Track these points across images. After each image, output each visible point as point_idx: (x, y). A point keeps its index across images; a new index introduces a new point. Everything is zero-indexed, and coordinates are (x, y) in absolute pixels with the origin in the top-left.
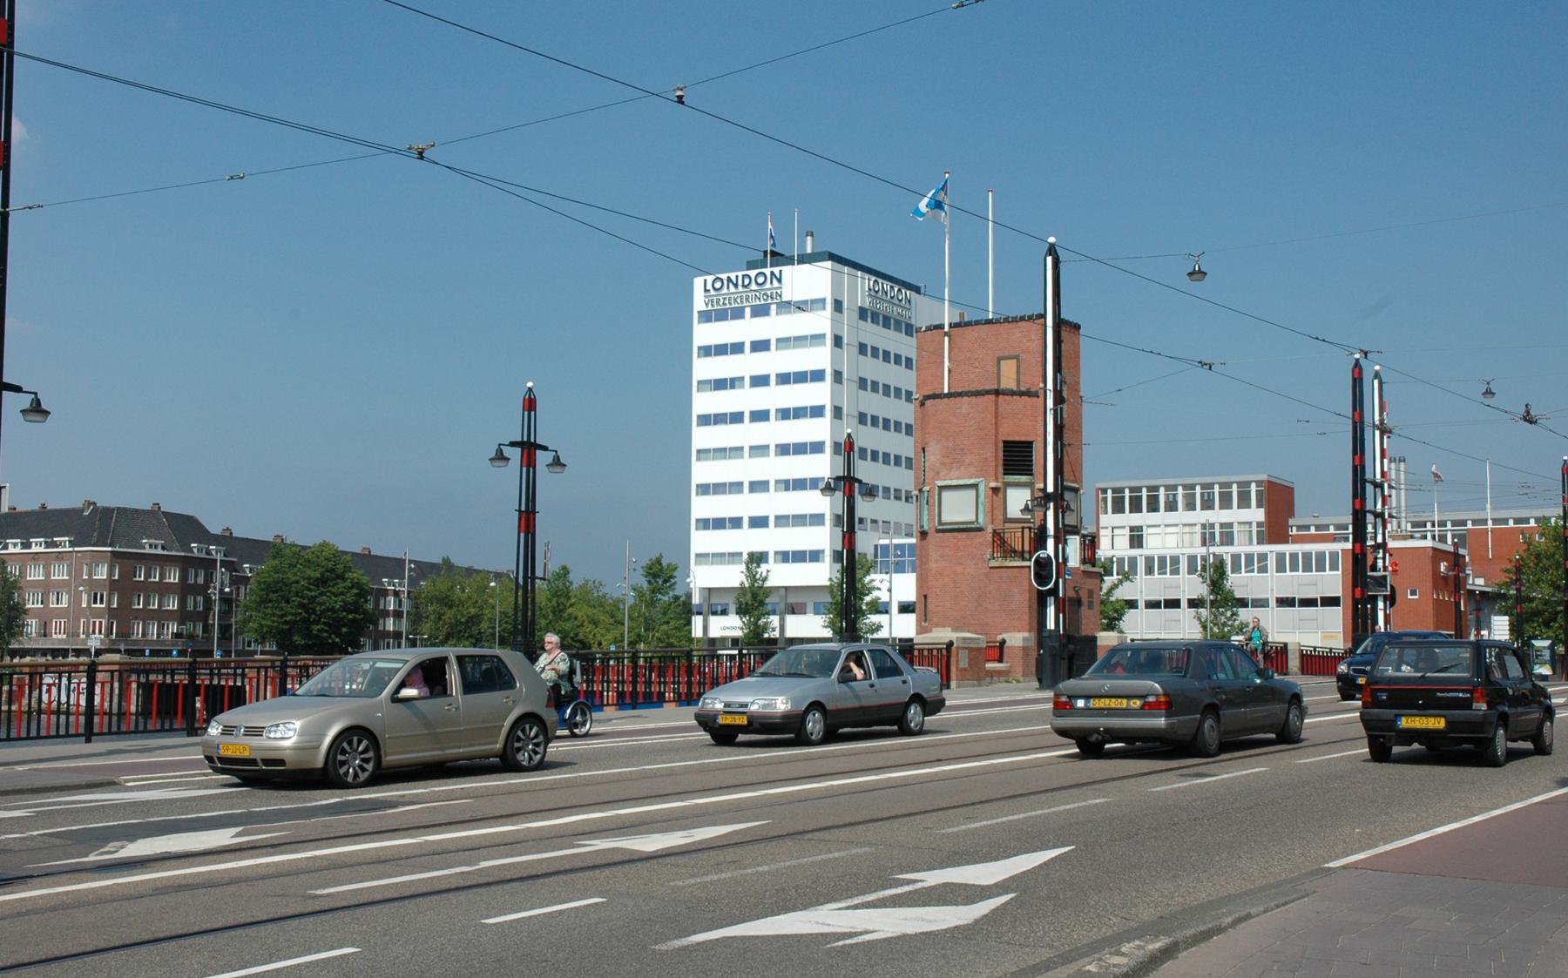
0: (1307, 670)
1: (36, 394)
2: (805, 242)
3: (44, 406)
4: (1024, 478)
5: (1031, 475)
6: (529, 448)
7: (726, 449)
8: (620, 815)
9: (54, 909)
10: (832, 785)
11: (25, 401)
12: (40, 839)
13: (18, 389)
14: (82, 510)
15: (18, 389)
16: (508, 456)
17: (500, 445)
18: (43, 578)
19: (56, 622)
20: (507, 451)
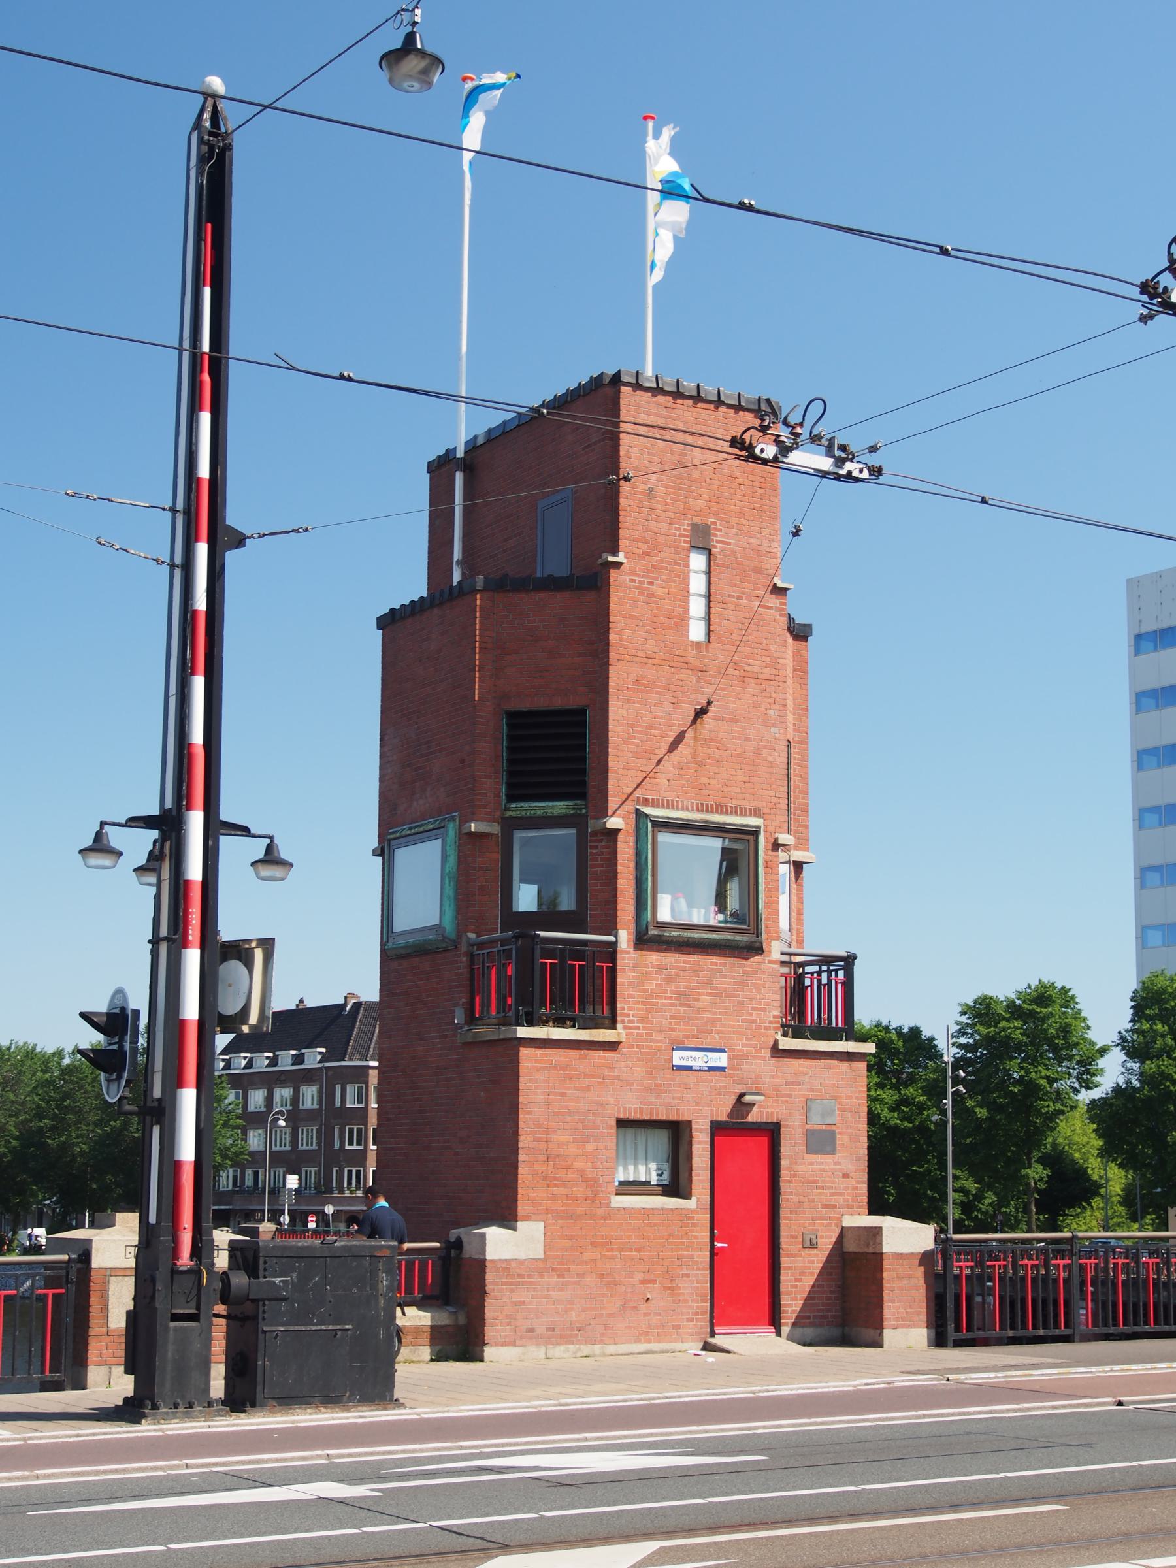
0: (1045, 1316)
1: (271, 838)
2: (201, 244)
3: (284, 854)
4: (559, 807)
5: (582, 796)
7: (1162, 866)
8: (712, 1502)
9: (982, 1503)
10: (1141, 1466)
11: (258, 849)
12: (1134, 1411)
13: (244, 831)
14: (344, 1006)
15: (244, 831)
16: (119, 847)
17: (103, 824)
18: (265, 1109)
19: (306, 1172)
20: (116, 837)
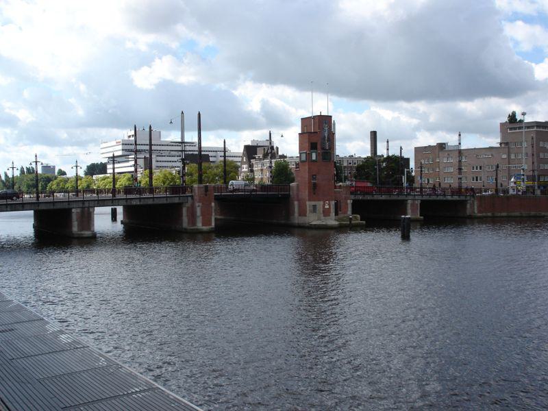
6: (77, 166)
